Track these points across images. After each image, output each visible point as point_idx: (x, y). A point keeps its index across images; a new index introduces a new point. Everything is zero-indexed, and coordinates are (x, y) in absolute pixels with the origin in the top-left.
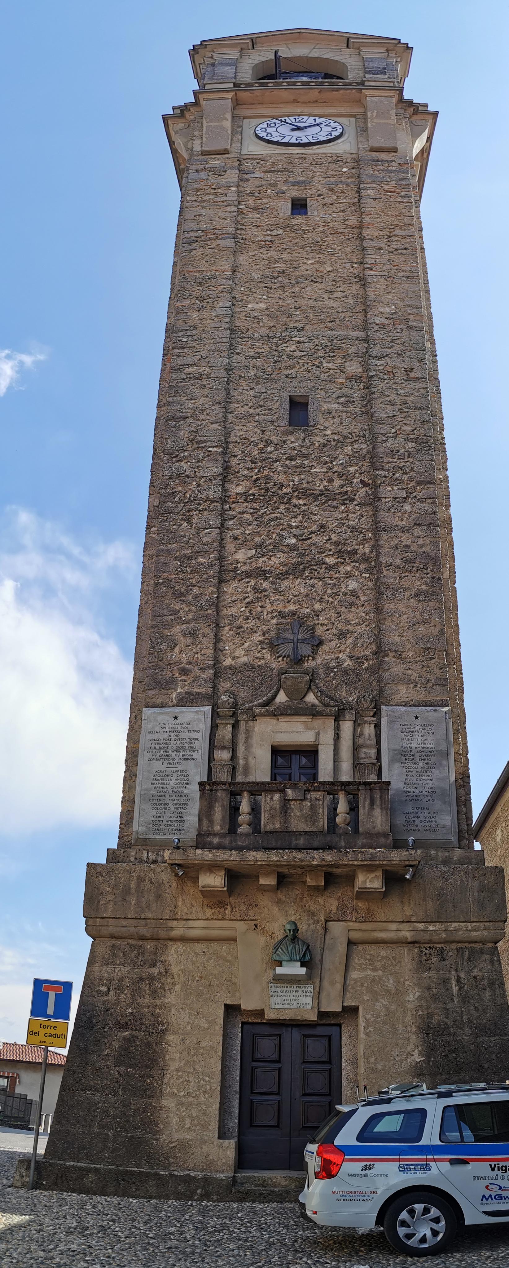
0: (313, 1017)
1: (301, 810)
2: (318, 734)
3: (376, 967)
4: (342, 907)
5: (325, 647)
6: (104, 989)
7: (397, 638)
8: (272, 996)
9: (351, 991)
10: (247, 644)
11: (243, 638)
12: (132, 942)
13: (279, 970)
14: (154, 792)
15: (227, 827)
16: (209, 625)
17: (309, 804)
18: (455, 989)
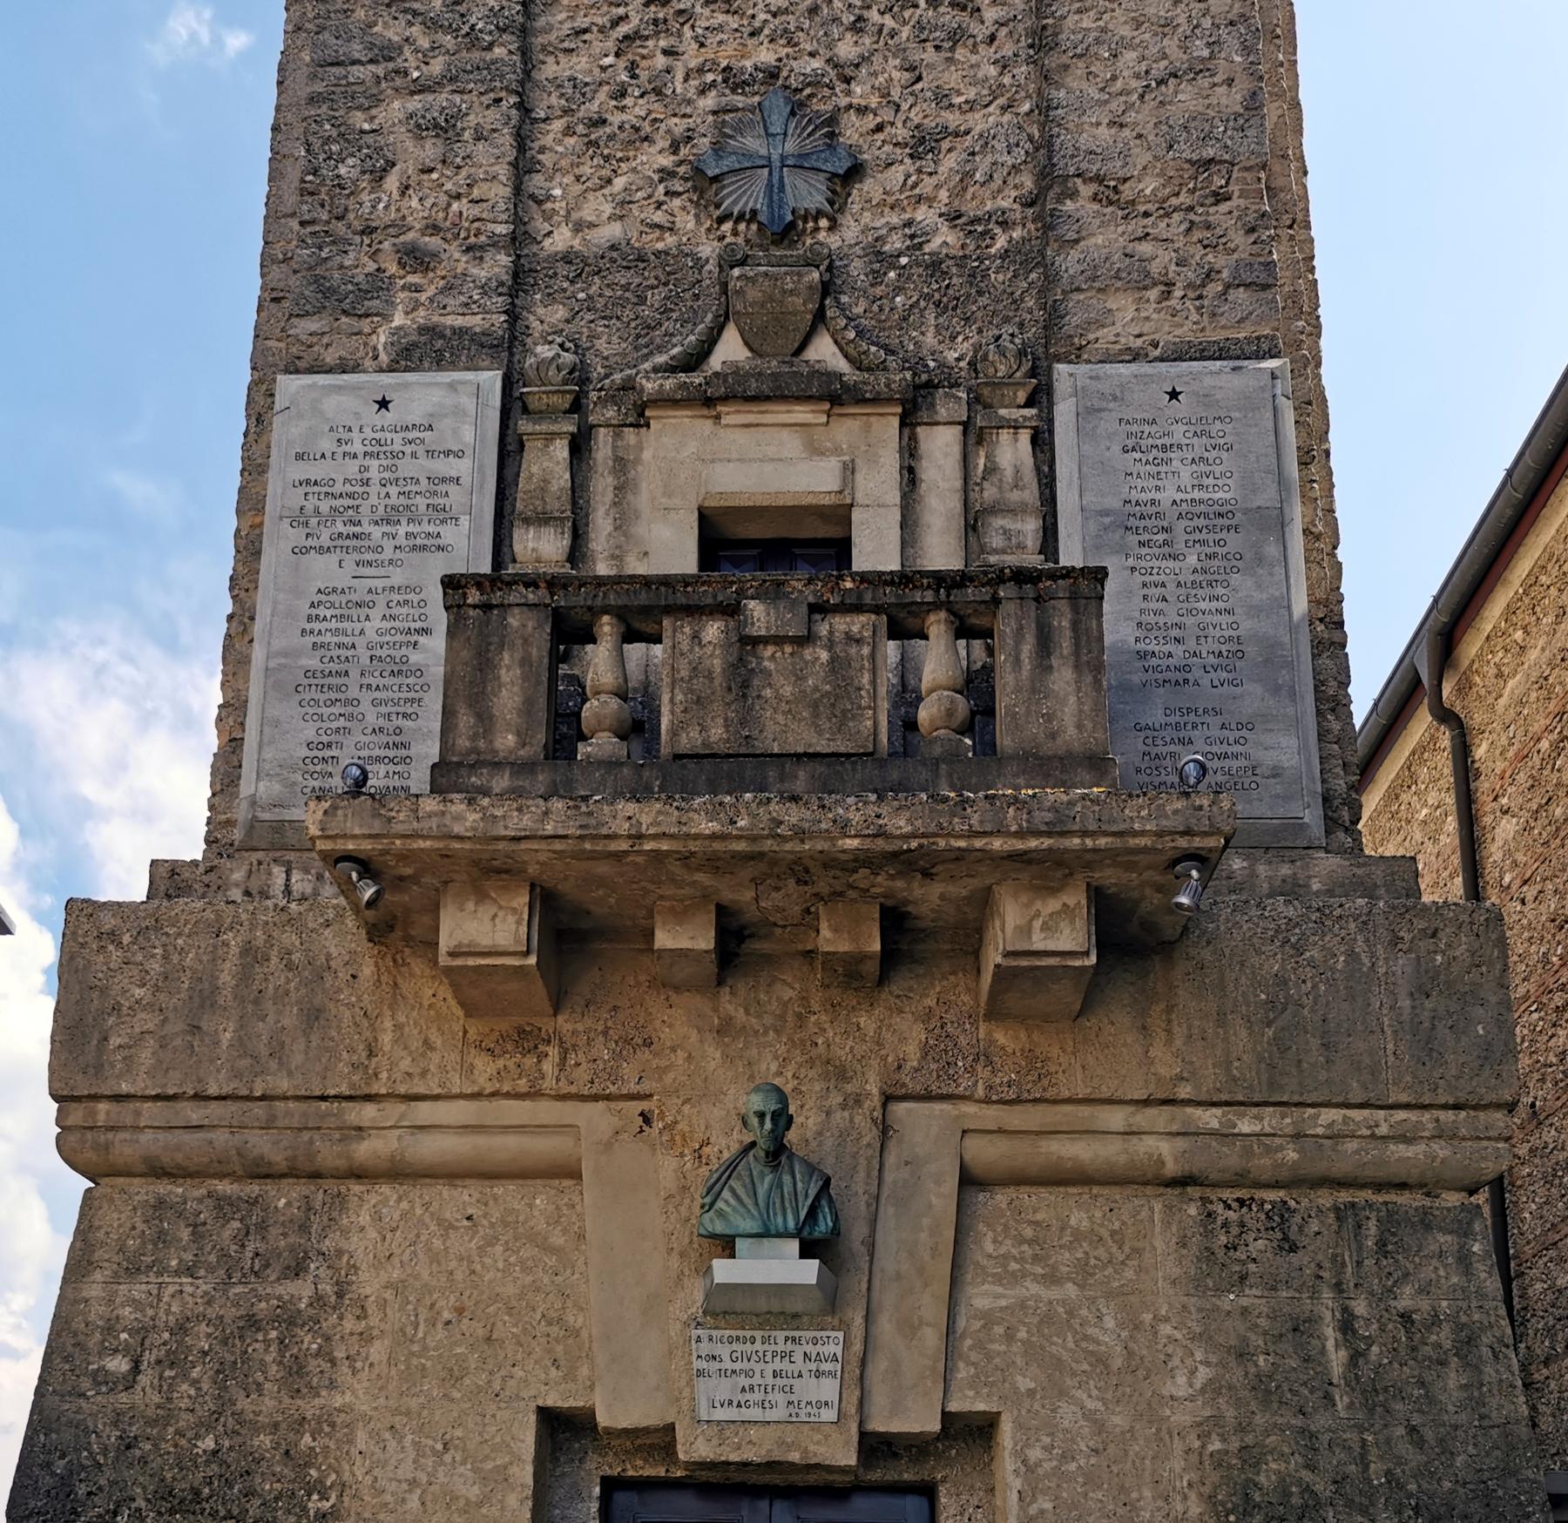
0: (847, 1457)
1: (800, 679)
2: (849, 470)
3: (1054, 1268)
4: (939, 1050)
5: (870, 187)
6: (119, 1365)
7: (1104, 133)
8: (700, 1373)
9: (974, 1357)
10: (619, 183)
11: (607, 158)
12: (224, 1187)
13: (724, 1271)
14: (313, 663)
15: (541, 737)
16: (498, 101)
17: (824, 656)
18: (1337, 1360)
